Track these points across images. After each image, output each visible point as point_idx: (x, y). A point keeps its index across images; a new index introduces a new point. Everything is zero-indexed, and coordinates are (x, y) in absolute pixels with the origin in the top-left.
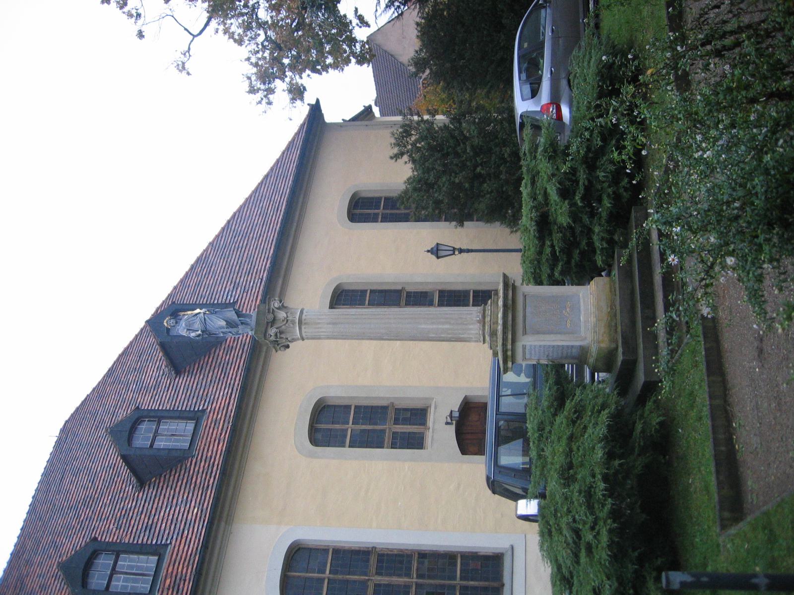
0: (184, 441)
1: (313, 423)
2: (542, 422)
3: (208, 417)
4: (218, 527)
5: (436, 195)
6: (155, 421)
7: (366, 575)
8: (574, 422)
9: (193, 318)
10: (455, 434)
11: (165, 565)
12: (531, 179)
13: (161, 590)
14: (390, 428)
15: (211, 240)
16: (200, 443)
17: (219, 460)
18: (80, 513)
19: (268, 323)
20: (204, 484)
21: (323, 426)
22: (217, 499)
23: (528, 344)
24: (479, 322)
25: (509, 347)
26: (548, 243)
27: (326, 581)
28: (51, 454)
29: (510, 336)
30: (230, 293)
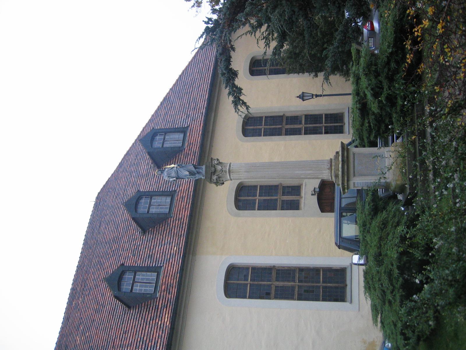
0: (166, 208)
1: (236, 197)
2: (365, 222)
3: (178, 195)
4: (188, 257)
5: (301, 61)
7: (270, 281)
8: (382, 230)
9: (171, 170)
10: (318, 205)
11: (161, 277)
12: (356, 81)
13: (160, 291)
14: (280, 198)
15: (171, 87)
16: (175, 209)
17: (186, 221)
18: (112, 246)
19: (212, 173)
20: (179, 234)
21: (242, 198)
22: (186, 243)
23: (356, 182)
24: (328, 169)
25: (346, 184)
26: (366, 121)
27: (249, 285)
28: (92, 212)
29: (346, 179)
30: (185, 121)
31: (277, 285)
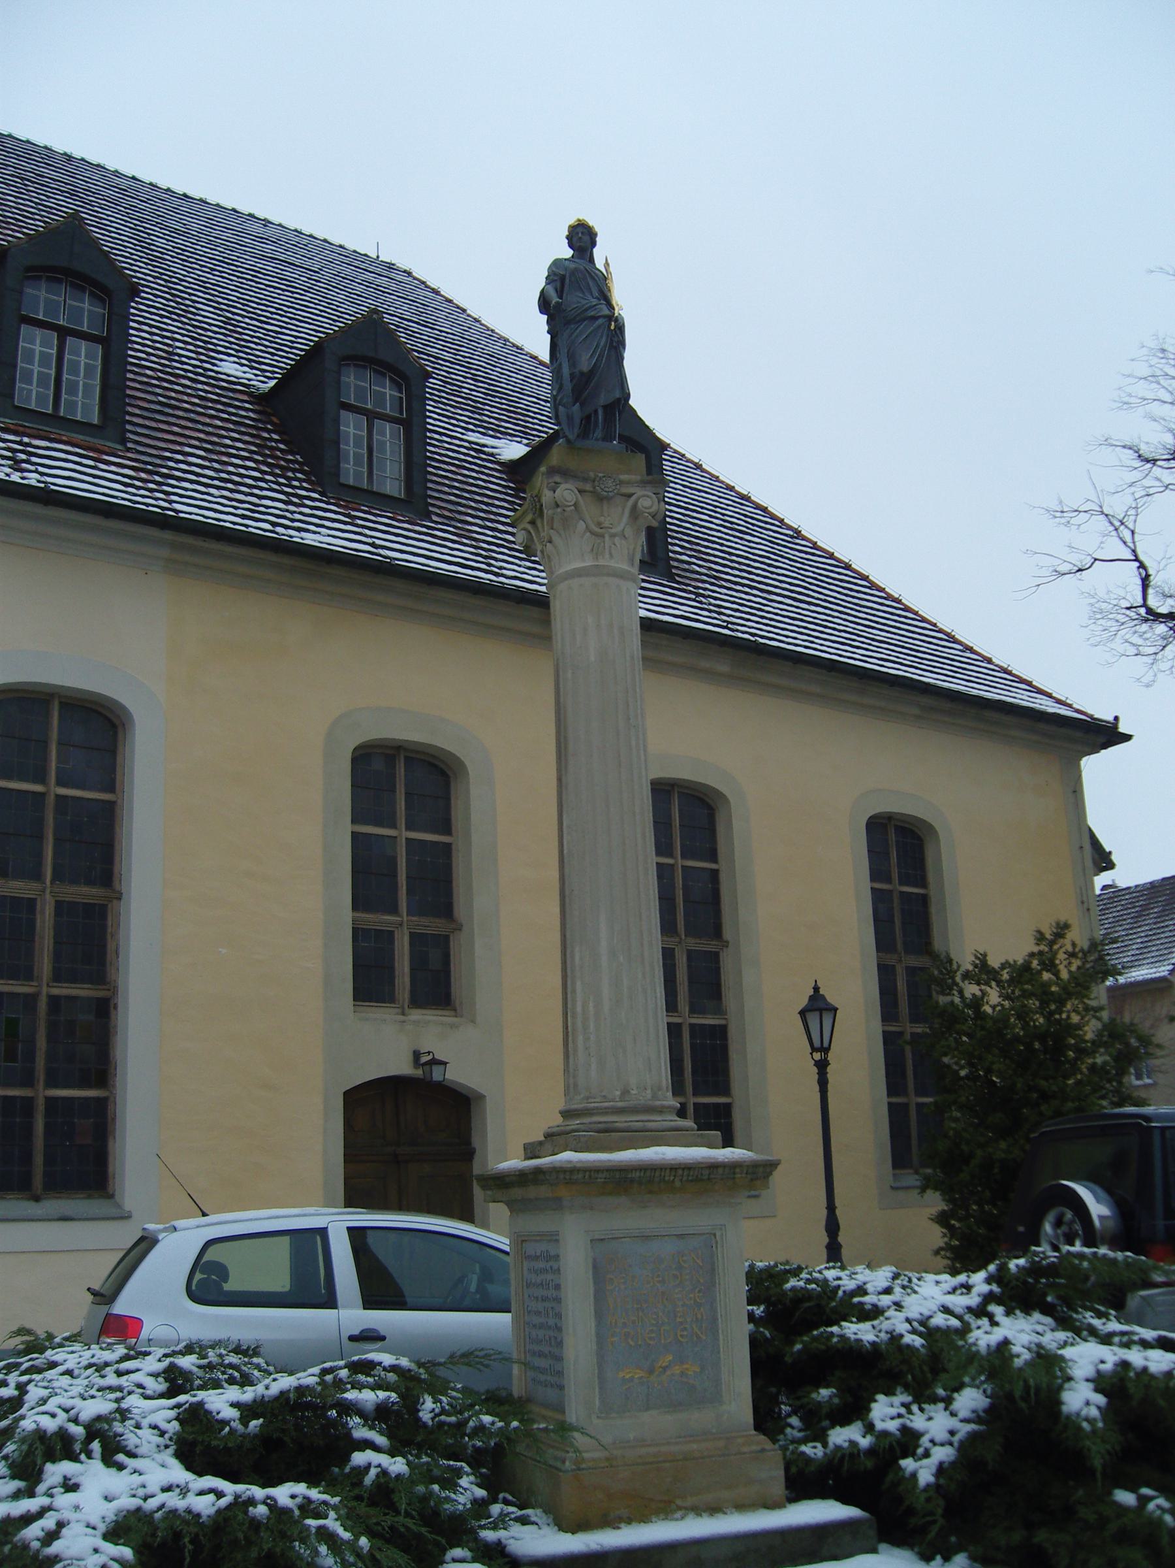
6: (402, 414)
27: (39, 788)
31: (38, 907)
